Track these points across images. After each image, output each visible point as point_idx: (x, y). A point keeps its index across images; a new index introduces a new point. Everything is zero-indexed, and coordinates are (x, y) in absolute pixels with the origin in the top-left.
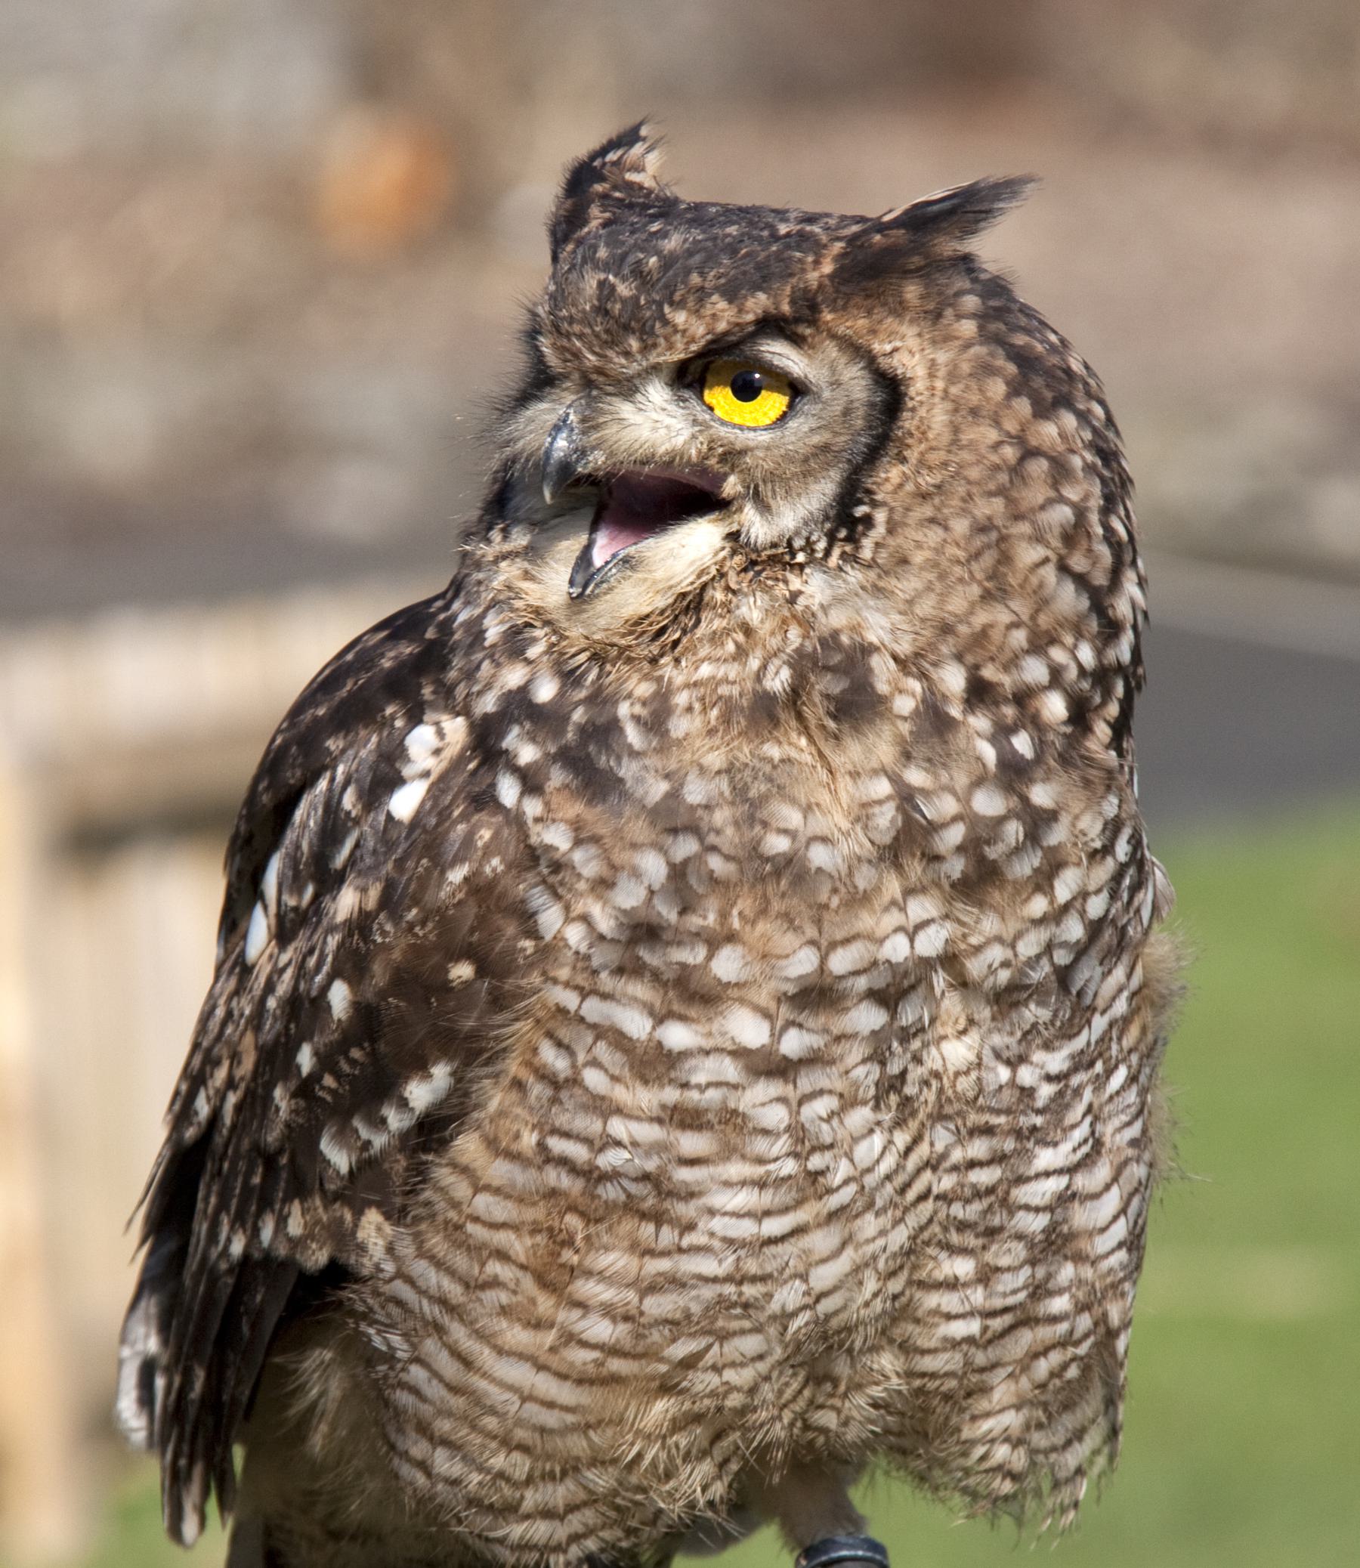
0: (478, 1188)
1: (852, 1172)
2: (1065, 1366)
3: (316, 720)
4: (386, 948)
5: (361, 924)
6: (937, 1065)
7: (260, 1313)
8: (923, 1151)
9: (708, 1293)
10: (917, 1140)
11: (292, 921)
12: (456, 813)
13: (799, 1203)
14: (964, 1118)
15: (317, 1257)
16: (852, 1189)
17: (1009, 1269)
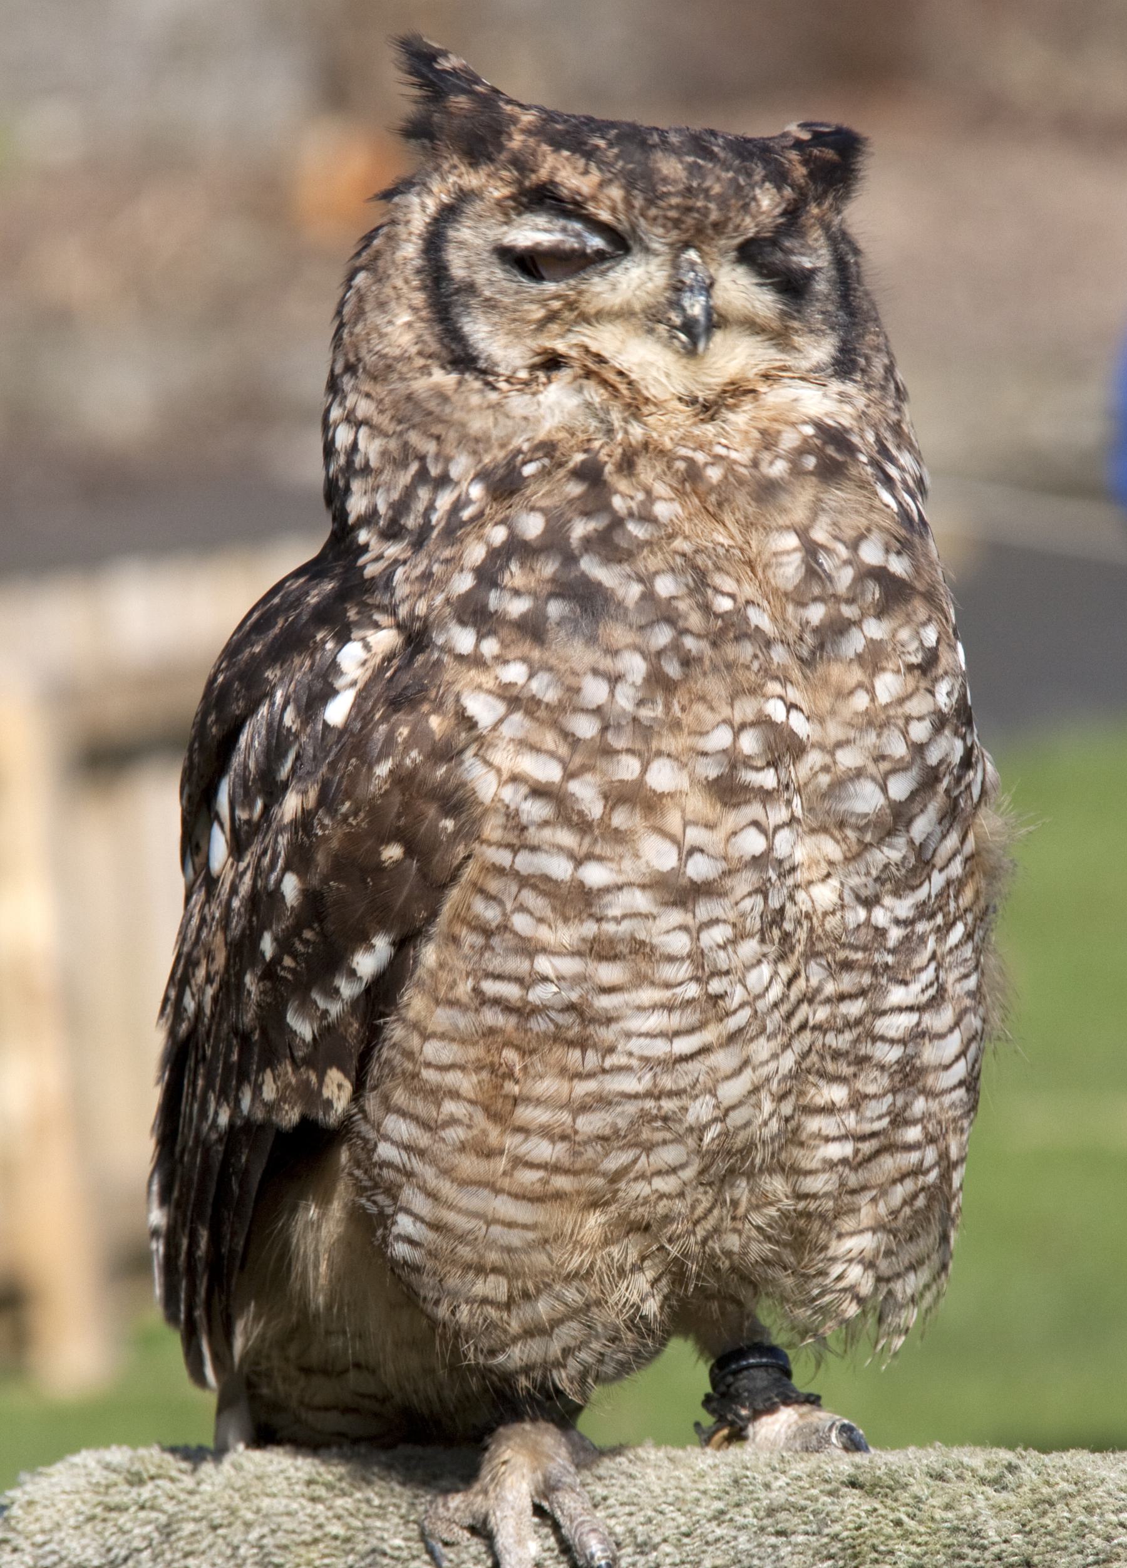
0: (426, 1037)
1: (746, 997)
2: (914, 1196)
3: (253, 656)
4: (326, 839)
5: (304, 822)
6: (806, 907)
7: (246, 1171)
8: (801, 984)
9: (631, 1108)
10: (795, 976)
11: (247, 832)
12: (377, 716)
13: (701, 1026)
14: (834, 955)
15: (291, 1116)
16: (746, 1013)
17: (875, 1096)
